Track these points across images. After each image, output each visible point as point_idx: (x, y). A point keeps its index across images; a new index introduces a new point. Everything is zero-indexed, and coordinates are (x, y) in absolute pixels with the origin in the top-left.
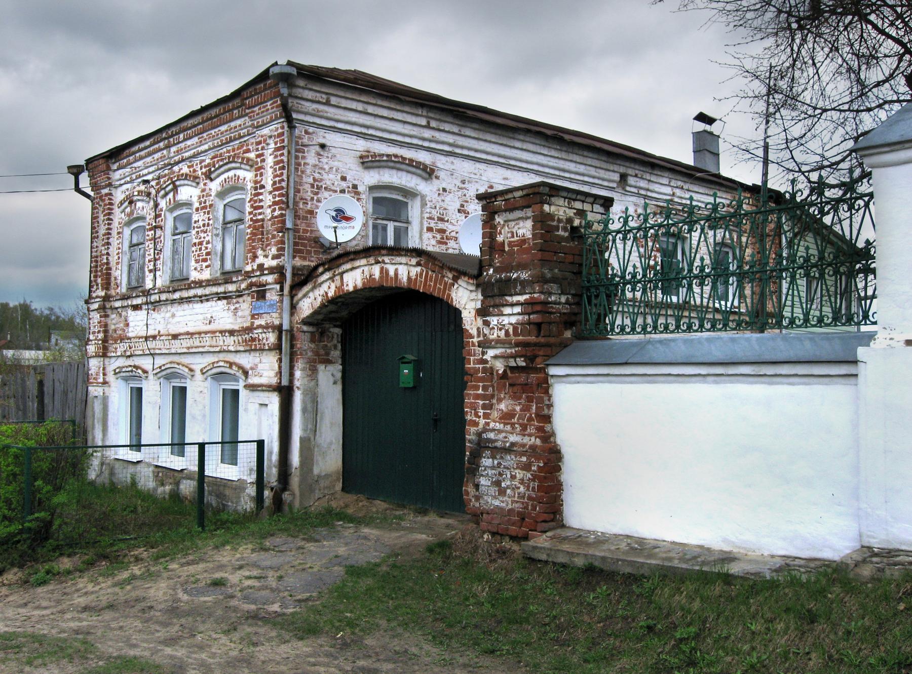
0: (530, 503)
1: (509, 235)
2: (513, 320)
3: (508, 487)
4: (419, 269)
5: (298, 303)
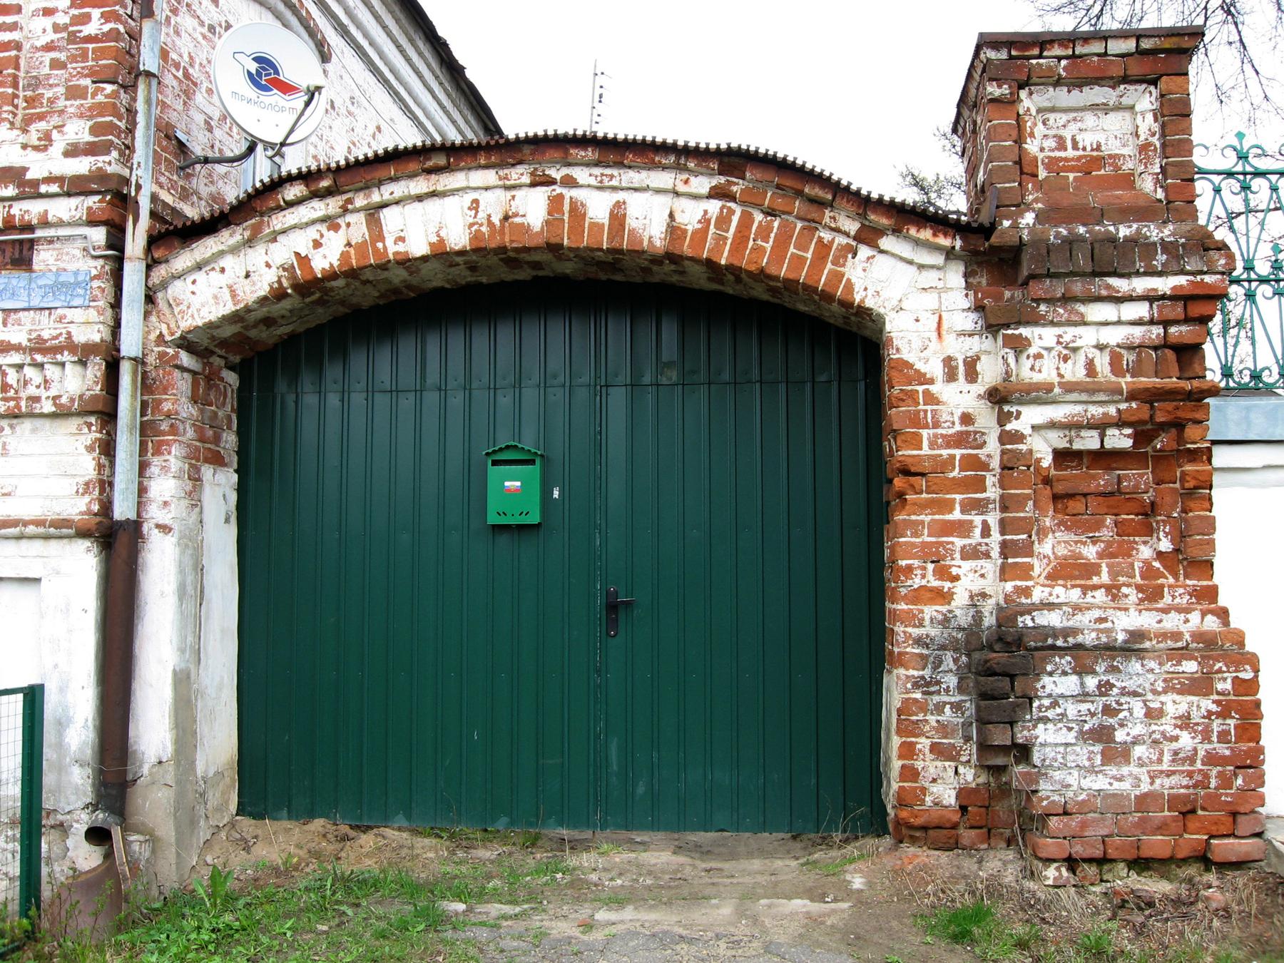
0: (1214, 771)
1: (1051, 143)
2: (1114, 336)
3: (1136, 741)
4: (714, 206)
5: (164, 285)
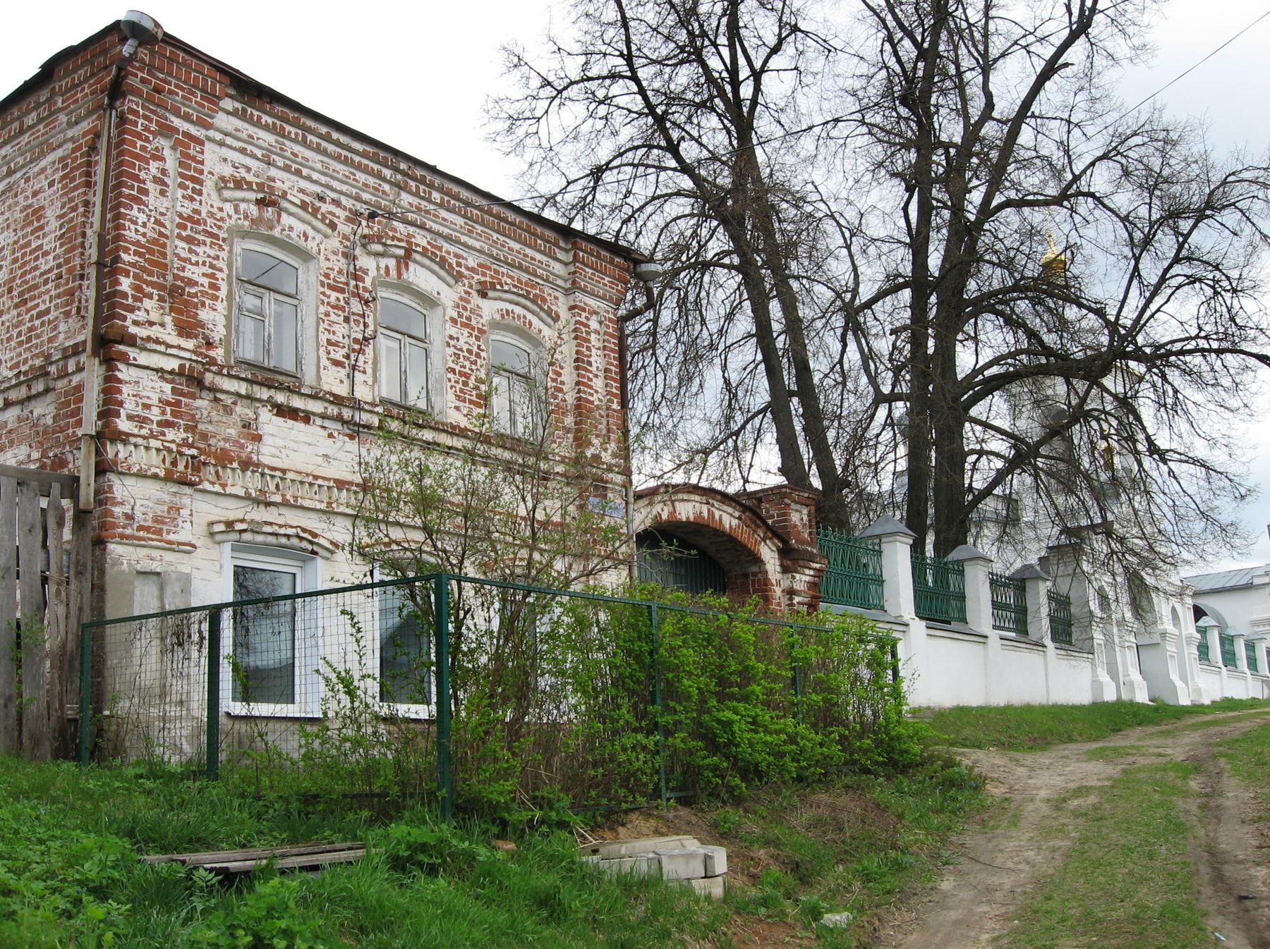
2: (808, 579)
